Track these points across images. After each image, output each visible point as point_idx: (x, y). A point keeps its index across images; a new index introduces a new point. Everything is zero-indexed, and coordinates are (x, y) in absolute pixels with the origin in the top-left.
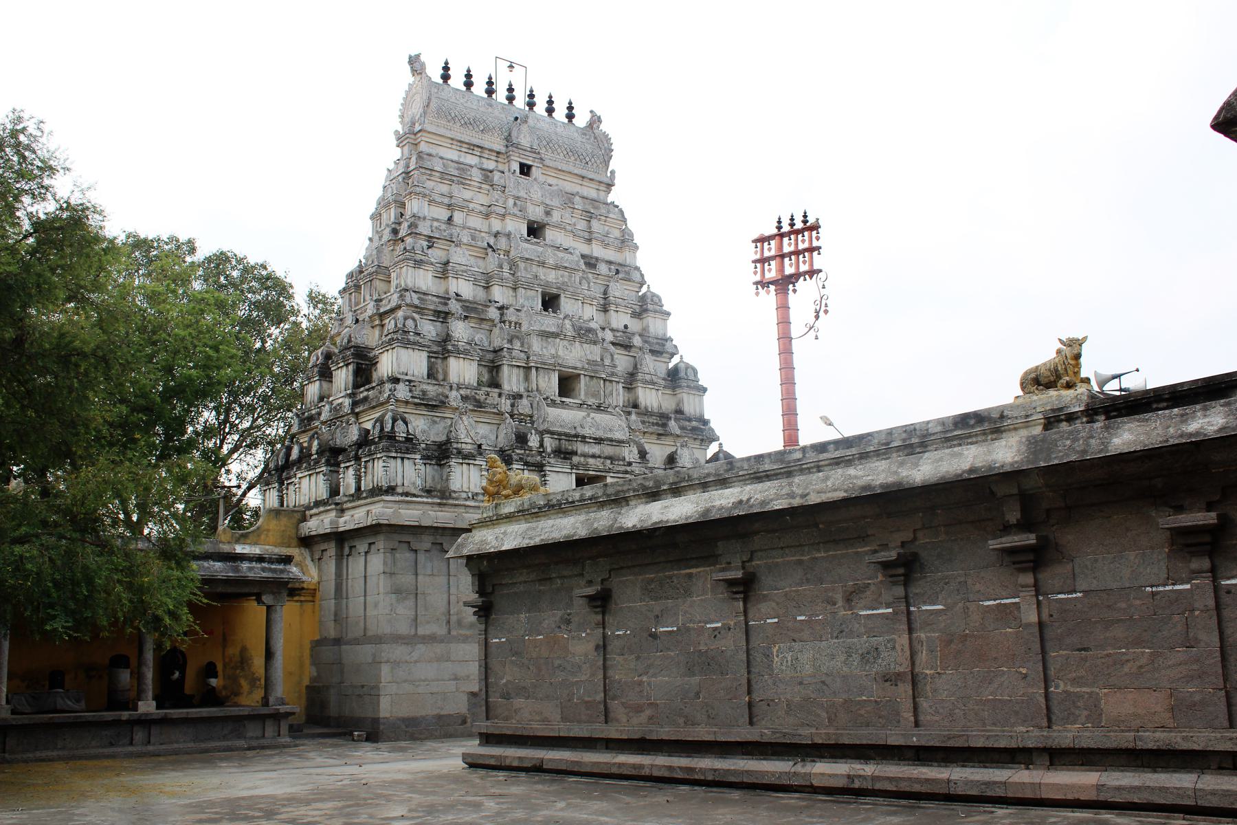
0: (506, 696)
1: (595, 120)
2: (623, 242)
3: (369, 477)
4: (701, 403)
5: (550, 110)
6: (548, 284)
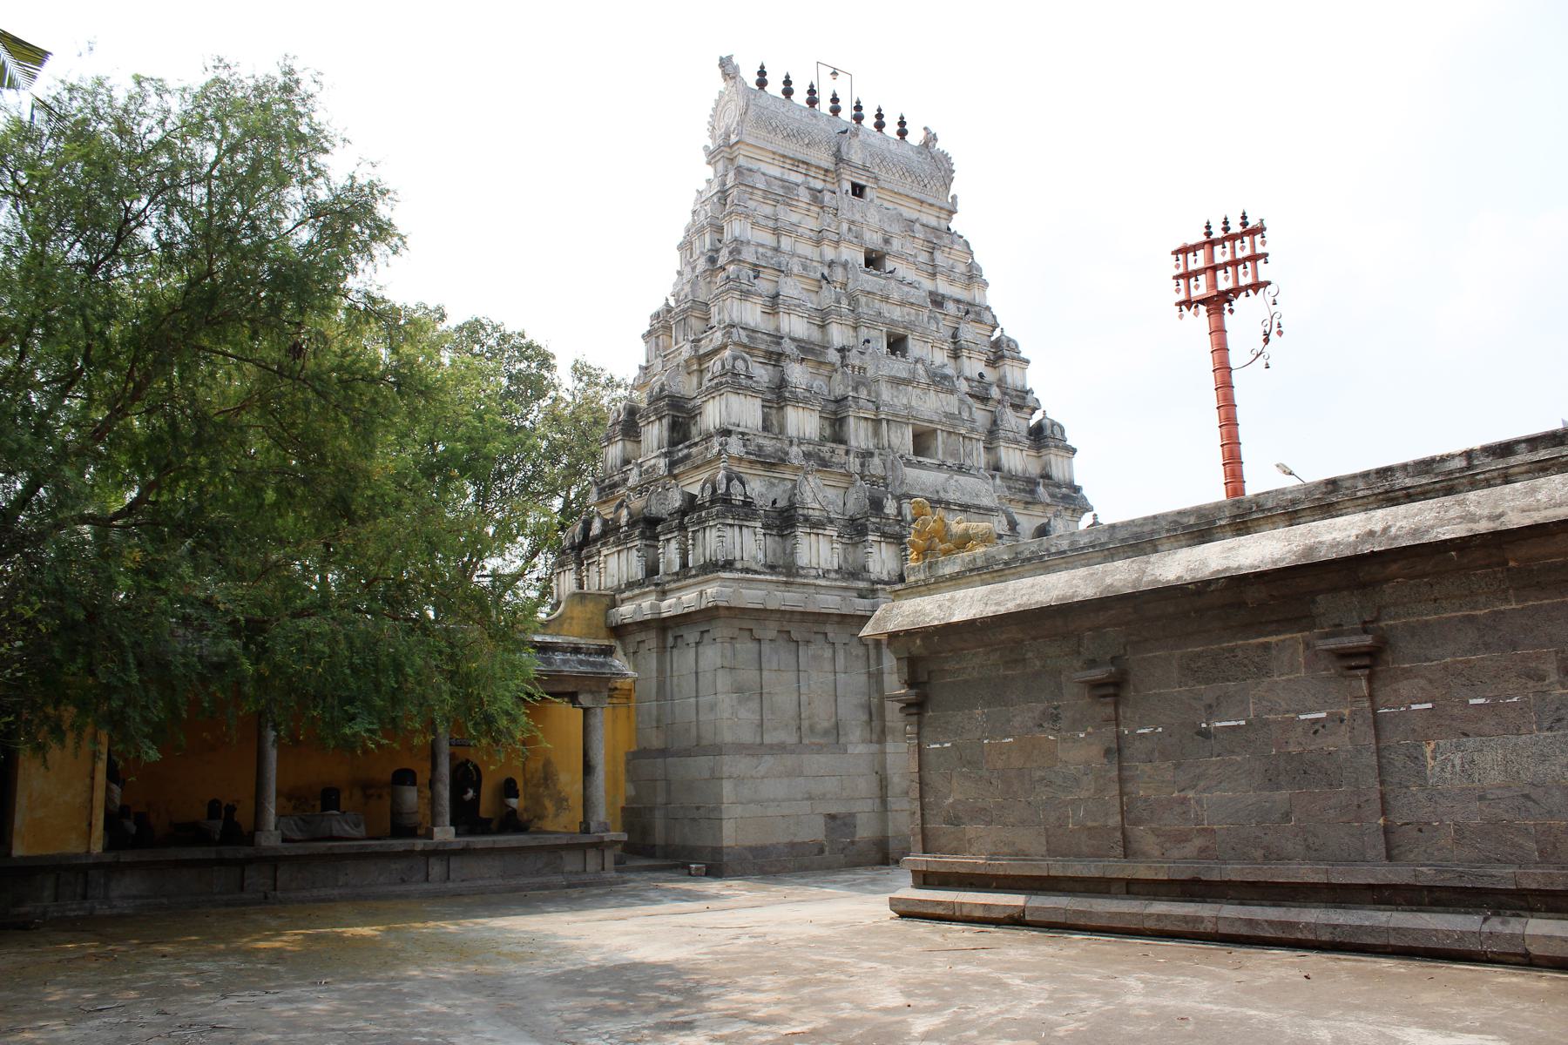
0: (955, 821)
1: (930, 139)
2: (970, 277)
3: (699, 550)
4: (1070, 466)
5: (880, 125)
6: (893, 322)
